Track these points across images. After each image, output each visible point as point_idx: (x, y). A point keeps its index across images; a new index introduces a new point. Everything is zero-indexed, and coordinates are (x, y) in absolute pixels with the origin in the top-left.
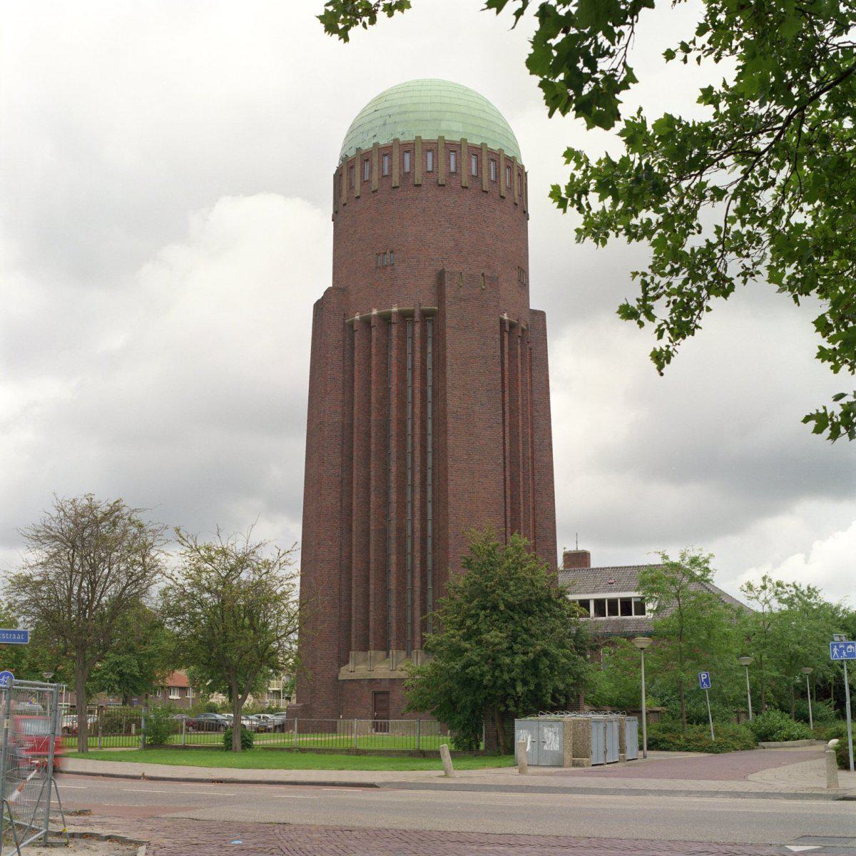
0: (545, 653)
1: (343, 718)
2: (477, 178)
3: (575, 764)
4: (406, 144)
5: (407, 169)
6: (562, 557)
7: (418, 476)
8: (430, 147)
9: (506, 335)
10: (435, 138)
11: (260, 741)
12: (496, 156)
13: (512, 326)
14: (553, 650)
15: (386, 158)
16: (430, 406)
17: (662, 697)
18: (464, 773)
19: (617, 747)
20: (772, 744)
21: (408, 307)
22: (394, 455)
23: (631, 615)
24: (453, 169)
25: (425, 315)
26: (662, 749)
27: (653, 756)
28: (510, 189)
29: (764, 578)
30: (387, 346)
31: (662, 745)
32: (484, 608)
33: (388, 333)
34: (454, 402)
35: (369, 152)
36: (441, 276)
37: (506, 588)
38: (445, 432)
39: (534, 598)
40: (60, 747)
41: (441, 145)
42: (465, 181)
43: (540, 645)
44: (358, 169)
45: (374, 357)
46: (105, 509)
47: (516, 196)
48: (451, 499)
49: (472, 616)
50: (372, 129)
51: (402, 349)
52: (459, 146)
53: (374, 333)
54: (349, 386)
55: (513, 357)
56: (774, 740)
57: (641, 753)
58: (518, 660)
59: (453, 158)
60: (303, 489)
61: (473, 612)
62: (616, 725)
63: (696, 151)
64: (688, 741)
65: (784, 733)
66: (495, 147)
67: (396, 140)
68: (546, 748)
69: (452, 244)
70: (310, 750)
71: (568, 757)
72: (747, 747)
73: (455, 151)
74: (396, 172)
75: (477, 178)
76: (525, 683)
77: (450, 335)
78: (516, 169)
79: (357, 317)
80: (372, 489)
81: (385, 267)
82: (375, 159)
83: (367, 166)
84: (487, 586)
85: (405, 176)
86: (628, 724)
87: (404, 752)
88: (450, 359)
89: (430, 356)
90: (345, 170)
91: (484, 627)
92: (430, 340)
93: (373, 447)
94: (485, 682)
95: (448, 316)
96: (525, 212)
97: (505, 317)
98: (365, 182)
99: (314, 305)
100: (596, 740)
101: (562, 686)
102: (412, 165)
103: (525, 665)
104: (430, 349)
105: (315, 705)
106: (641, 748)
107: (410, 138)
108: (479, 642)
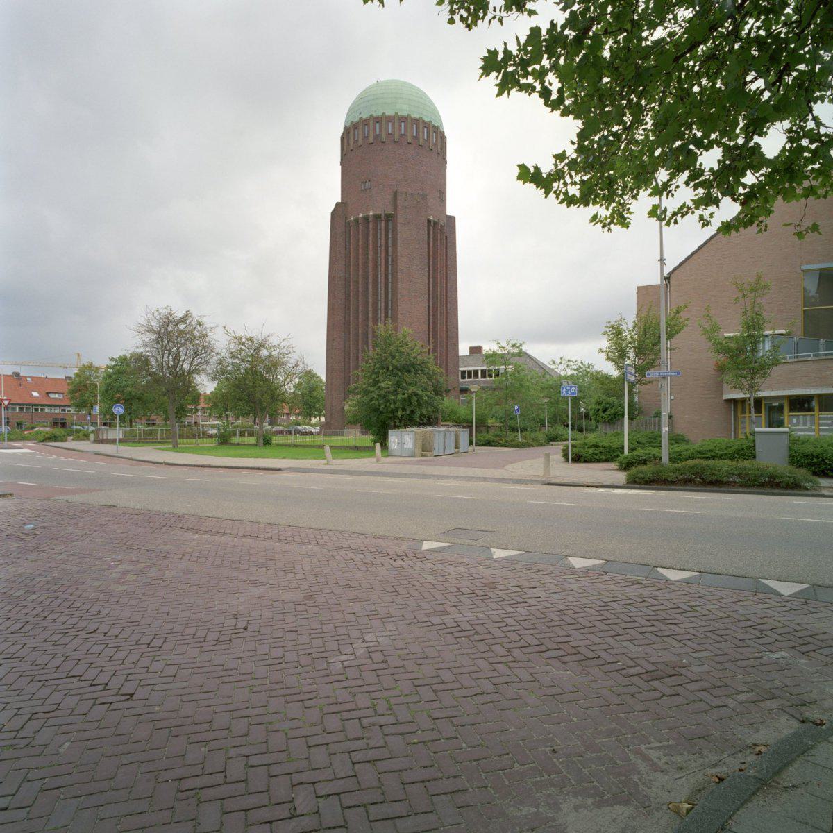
0: (416, 394)
2: (416, 138)
3: (423, 456)
4: (377, 118)
5: (378, 133)
7: (383, 304)
8: (390, 119)
9: (432, 228)
10: (393, 113)
11: (276, 440)
12: (427, 125)
13: (435, 223)
14: (420, 392)
15: (366, 127)
16: (390, 267)
17: (500, 419)
18: (339, 461)
19: (453, 445)
20: (556, 443)
21: (378, 212)
22: (371, 294)
23: (755, 413)
24: (403, 132)
25: (388, 217)
26: (492, 446)
27: (482, 450)
29: (561, 358)
30: (367, 235)
31: (493, 444)
32: (383, 368)
33: (368, 227)
34: (401, 264)
35: (357, 123)
36: (395, 194)
37: (394, 357)
38: (397, 280)
39: (408, 363)
40: (770, 411)
41: (396, 118)
42: (409, 139)
43: (411, 390)
44: (351, 133)
45: (360, 240)
46: (181, 315)
47: (439, 150)
48: (399, 316)
49: (376, 373)
50: (359, 109)
51: (375, 236)
52: (406, 118)
53: (360, 227)
54: (347, 256)
55: (435, 240)
56: (558, 441)
57: (470, 449)
58: (399, 397)
61: (376, 370)
62: (453, 434)
64: (507, 442)
65: (563, 437)
66: (427, 120)
67: (371, 116)
68: (405, 446)
69: (402, 176)
70: (300, 446)
71: (419, 451)
72: (541, 445)
74: (371, 135)
75: (416, 138)
76: (404, 409)
77: (400, 227)
79: (352, 219)
80: (360, 311)
81: (366, 190)
83: (356, 131)
84: (547, 380)
85: (377, 137)
86: (462, 433)
87: (347, 447)
88: (399, 241)
89: (390, 240)
90: (345, 134)
91: (381, 379)
92: (390, 231)
93: (360, 290)
94: (381, 410)
95: (399, 217)
96: (444, 159)
97: (431, 218)
98: (355, 141)
99: (334, 214)
100: (438, 443)
101: (425, 413)
102: (380, 131)
103: (404, 400)
104: (390, 236)
105: (332, 422)
106: (471, 443)
107: (379, 114)
108: (379, 388)
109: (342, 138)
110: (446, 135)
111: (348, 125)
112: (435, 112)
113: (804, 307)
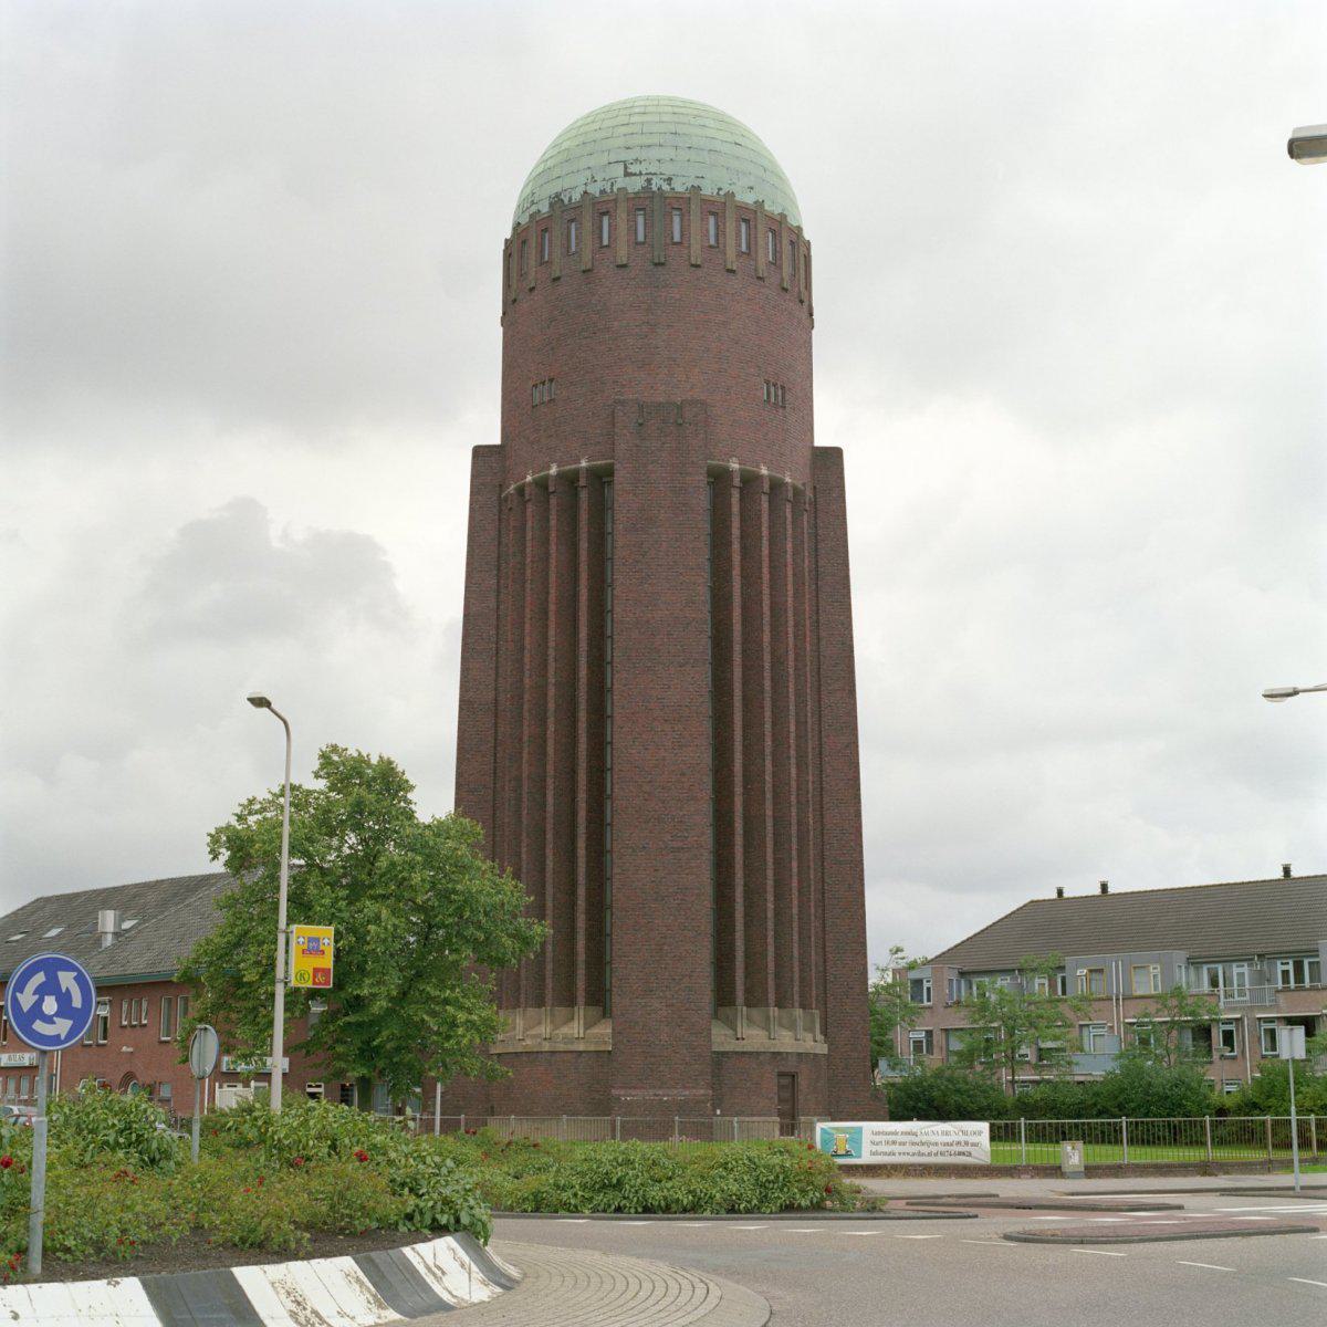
1: (722, 1115)
6: (1093, 1181)
28: (776, 263)
35: (578, 207)
42: (696, 254)
59: (640, 220)
60: (455, 760)
63: (124, 1049)
73: (644, 209)
78: (785, 234)
82: (622, 215)
109: (508, 255)
110: (807, 235)
111: (524, 220)
112: (769, 171)
113: (1318, 962)
